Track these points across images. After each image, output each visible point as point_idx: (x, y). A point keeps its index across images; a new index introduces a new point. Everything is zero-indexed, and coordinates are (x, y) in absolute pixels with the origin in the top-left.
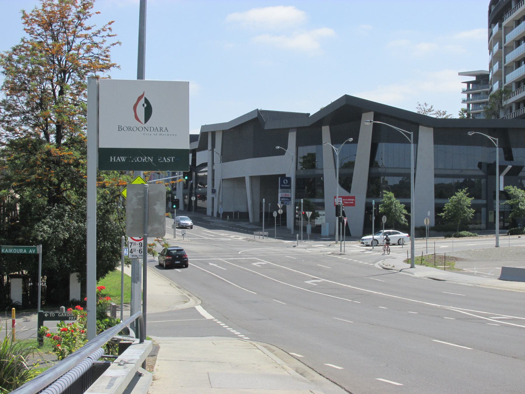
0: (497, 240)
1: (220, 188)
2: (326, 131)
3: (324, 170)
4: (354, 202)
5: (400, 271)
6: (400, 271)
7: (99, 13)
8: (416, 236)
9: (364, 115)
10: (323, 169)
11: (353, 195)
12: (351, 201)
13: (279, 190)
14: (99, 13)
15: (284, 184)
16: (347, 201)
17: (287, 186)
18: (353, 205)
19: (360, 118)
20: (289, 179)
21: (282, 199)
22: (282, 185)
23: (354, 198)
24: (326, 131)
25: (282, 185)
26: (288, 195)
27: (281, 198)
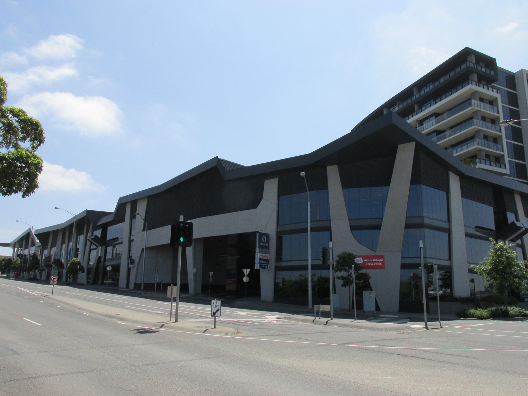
0: (426, 325)
1: (140, 258)
2: (333, 175)
3: (332, 222)
4: (383, 263)
5: (162, 326)
6: (162, 326)
7: (56, 208)
8: (180, 301)
9: (400, 147)
10: (330, 220)
11: (382, 254)
12: (378, 262)
13: (257, 250)
14: (56, 208)
15: (263, 242)
16: (370, 262)
17: (265, 244)
18: (382, 267)
19: (393, 152)
20: (267, 236)
21: (261, 261)
22: (261, 244)
23: (382, 257)
24: (333, 175)
25: (261, 244)
26: (267, 256)
27: (260, 259)
